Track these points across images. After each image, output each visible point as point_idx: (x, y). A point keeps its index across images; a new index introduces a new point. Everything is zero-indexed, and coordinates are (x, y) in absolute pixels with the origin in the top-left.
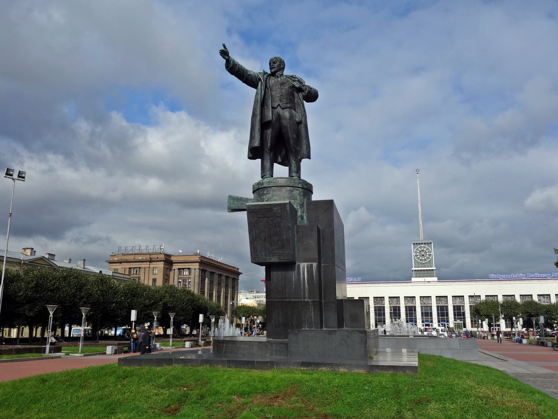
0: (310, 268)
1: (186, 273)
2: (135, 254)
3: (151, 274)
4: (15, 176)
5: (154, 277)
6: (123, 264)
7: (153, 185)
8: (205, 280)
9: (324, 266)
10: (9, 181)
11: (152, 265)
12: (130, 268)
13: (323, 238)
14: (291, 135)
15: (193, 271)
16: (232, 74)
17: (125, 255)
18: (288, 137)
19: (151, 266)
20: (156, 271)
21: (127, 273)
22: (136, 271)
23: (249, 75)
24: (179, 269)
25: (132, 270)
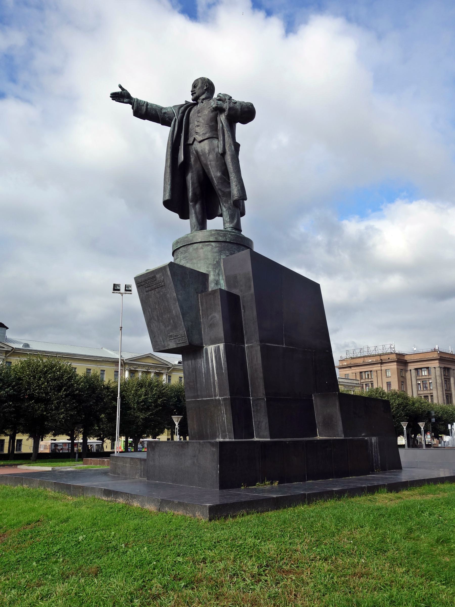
0: (217, 351)
1: (425, 373)
2: (364, 357)
3: (384, 378)
4: (122, 289)
5: (388, 380)
6: (353, 368)
7: (395, 282)
8: (450, 379)
9: (248, 347)
10: (117, 295)
11: (384, 367)
12: (361, 373)
13: (244, 307)
14: (215, 174)
15: (432, 371)
16: (144, 119)
17: (354, 358)
18: (212, 178)
19: (383, 368)
20: (389, 374)
21: (358, 378)
22: (368, 375)
23: (165, 113)
24: (416, 369)
25: (363, 374)
